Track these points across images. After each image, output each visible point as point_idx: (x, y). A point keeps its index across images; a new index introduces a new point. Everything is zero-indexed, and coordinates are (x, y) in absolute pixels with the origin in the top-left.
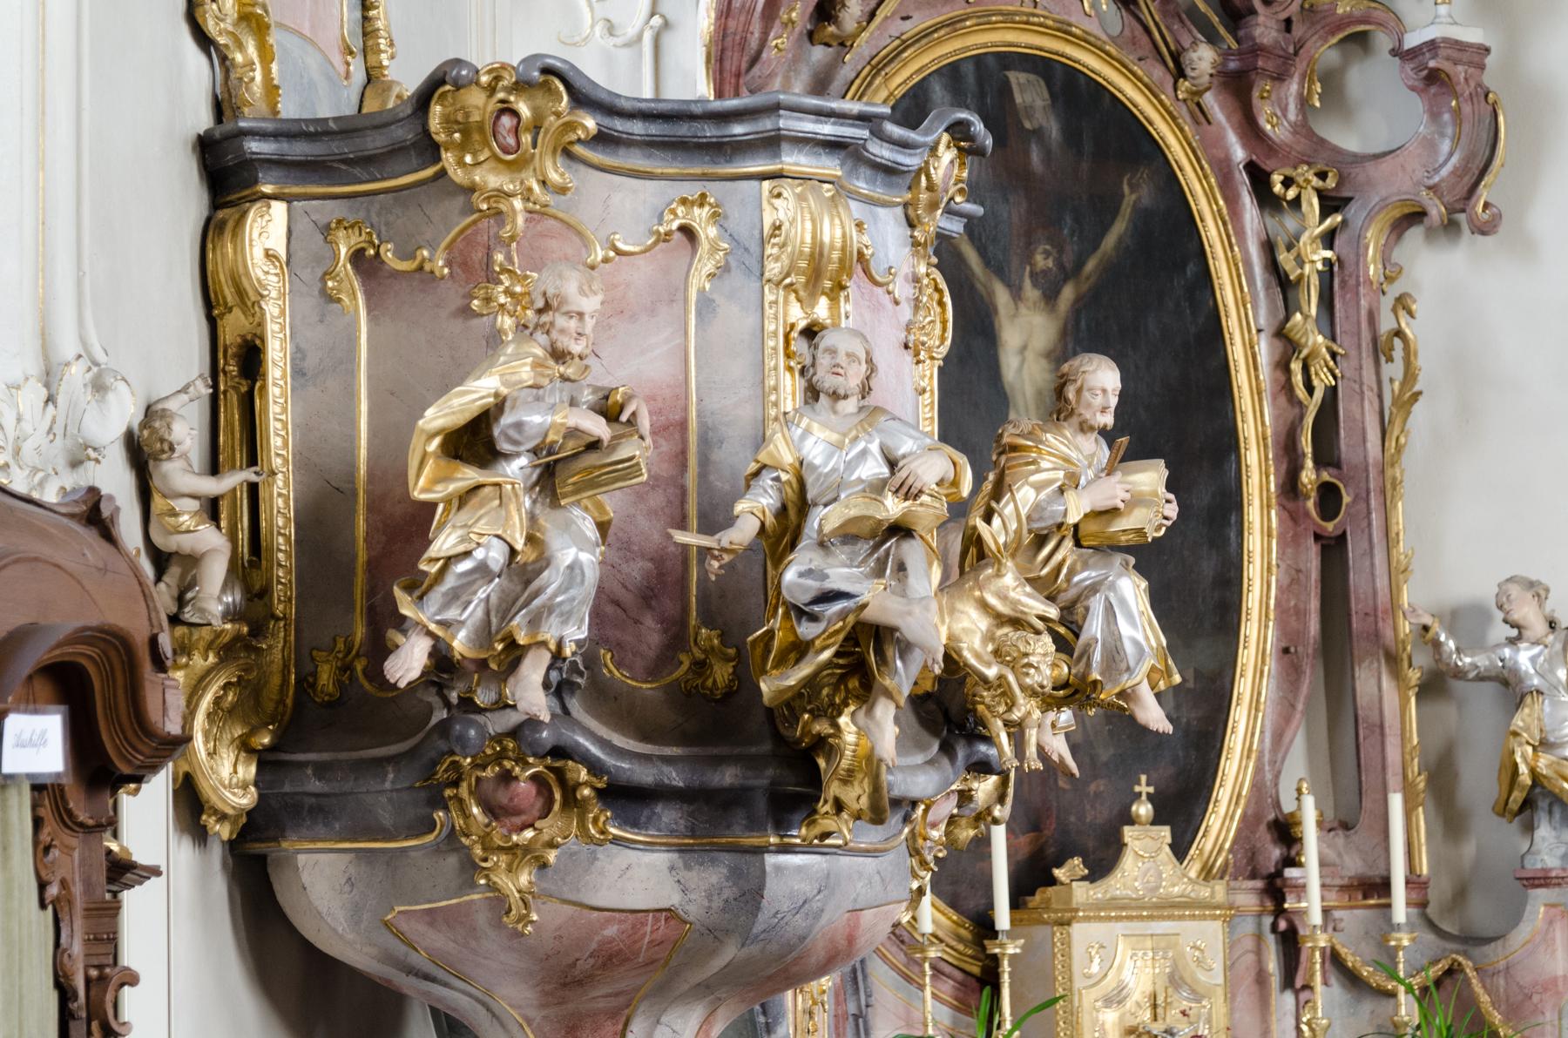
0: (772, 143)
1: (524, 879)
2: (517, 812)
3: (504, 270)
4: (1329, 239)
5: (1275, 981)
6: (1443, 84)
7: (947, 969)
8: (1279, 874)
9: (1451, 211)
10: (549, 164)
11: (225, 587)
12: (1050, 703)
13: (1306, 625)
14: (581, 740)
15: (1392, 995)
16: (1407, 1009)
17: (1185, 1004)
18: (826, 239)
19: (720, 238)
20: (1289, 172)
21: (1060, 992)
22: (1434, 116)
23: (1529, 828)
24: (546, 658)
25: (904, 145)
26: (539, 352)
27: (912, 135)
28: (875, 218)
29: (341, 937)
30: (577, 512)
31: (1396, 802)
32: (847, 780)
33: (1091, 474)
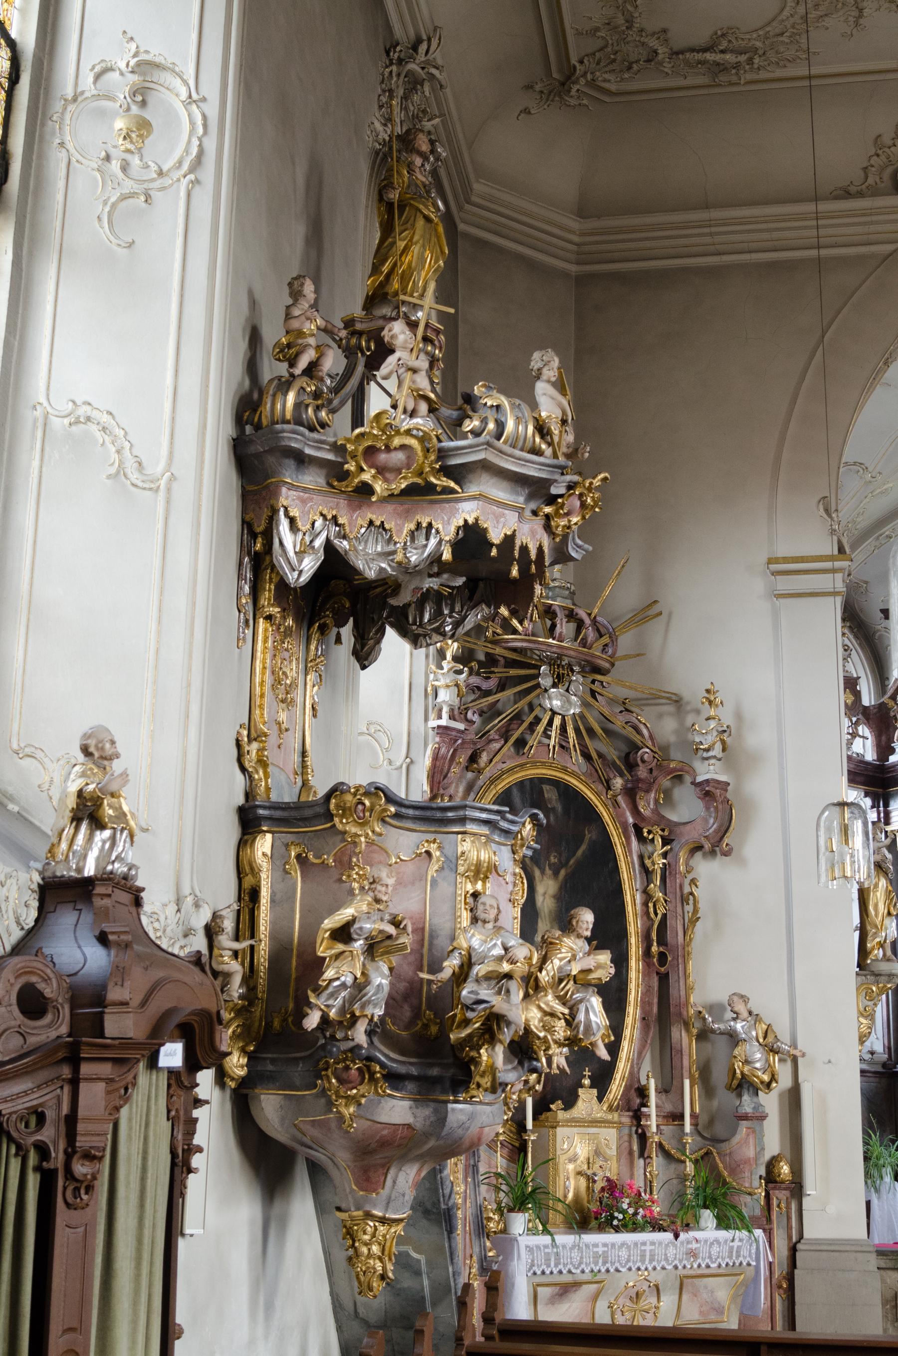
0: (463, 820)
1: (352, 1109)
2: (350, 1082)
3: (356, 865)
4: (665, 855)
5: (636, 1154)
6: (711, 796)
7: (506, 1144)
8: (639, 1110)
9: (713, 846)
10: (376, 824)
11: (240, 986)
12: (560, 1044)
13: (652, 1010)
14: (378, 1054)
15: (684, 1162)
16: (690, 1168)
17: (601, 1163)
18: (482, 858)
19: (441, 856)
20: (650, 828)
21: (551, 1156)
22: (707, 808)
23: (740, 1096)
24: (367, 1021)
25: (513, 822)
26: (370, 899)
27: (516, 819)
28: (500, 850)
29: (276, 1129)
30: (381, 963)
31: (687, 1082)
32: (482, 1076)
33: (581, 955)
